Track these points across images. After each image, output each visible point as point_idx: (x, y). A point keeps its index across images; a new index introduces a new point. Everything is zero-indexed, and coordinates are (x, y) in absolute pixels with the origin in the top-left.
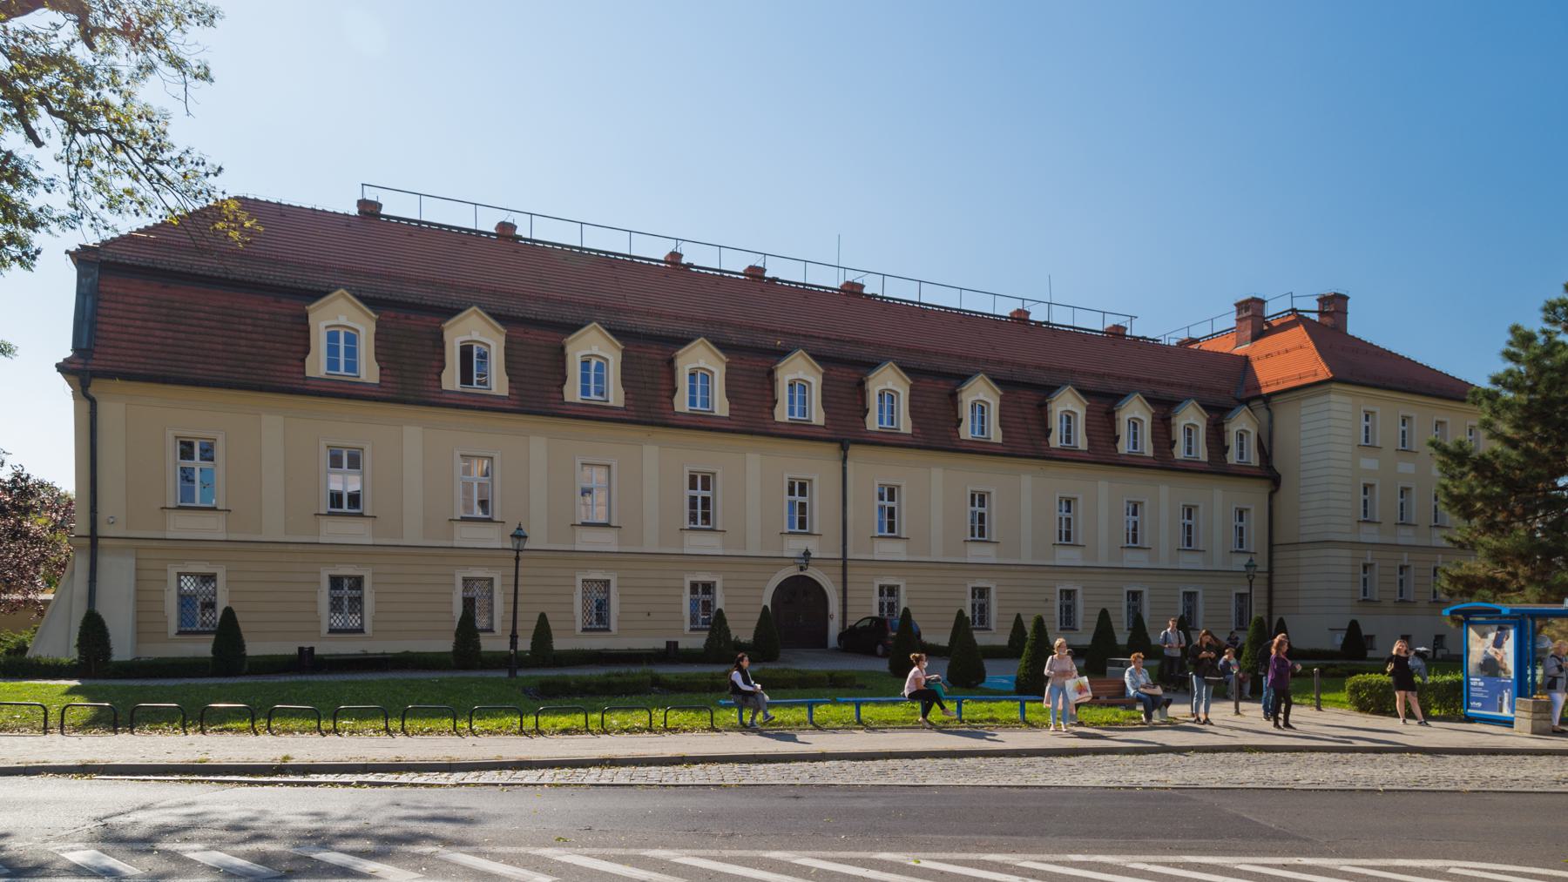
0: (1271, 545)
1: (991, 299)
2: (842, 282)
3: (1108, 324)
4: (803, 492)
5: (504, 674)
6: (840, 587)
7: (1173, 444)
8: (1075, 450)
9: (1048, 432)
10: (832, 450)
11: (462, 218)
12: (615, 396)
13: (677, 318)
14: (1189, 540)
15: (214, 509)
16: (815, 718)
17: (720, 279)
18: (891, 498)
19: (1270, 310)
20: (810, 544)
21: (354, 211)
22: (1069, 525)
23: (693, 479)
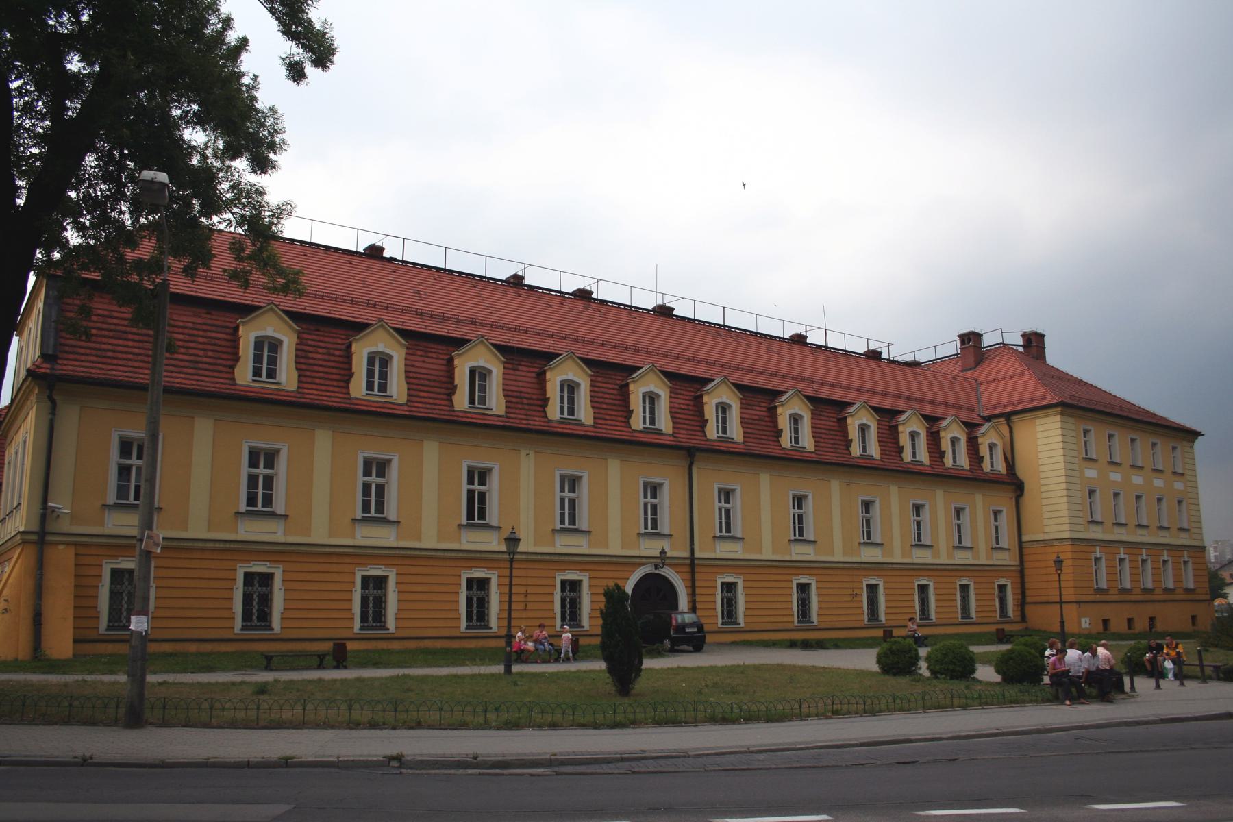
5: (499, 669)
9: (704, 422)
13: (832, 385)
19: (987, 341)
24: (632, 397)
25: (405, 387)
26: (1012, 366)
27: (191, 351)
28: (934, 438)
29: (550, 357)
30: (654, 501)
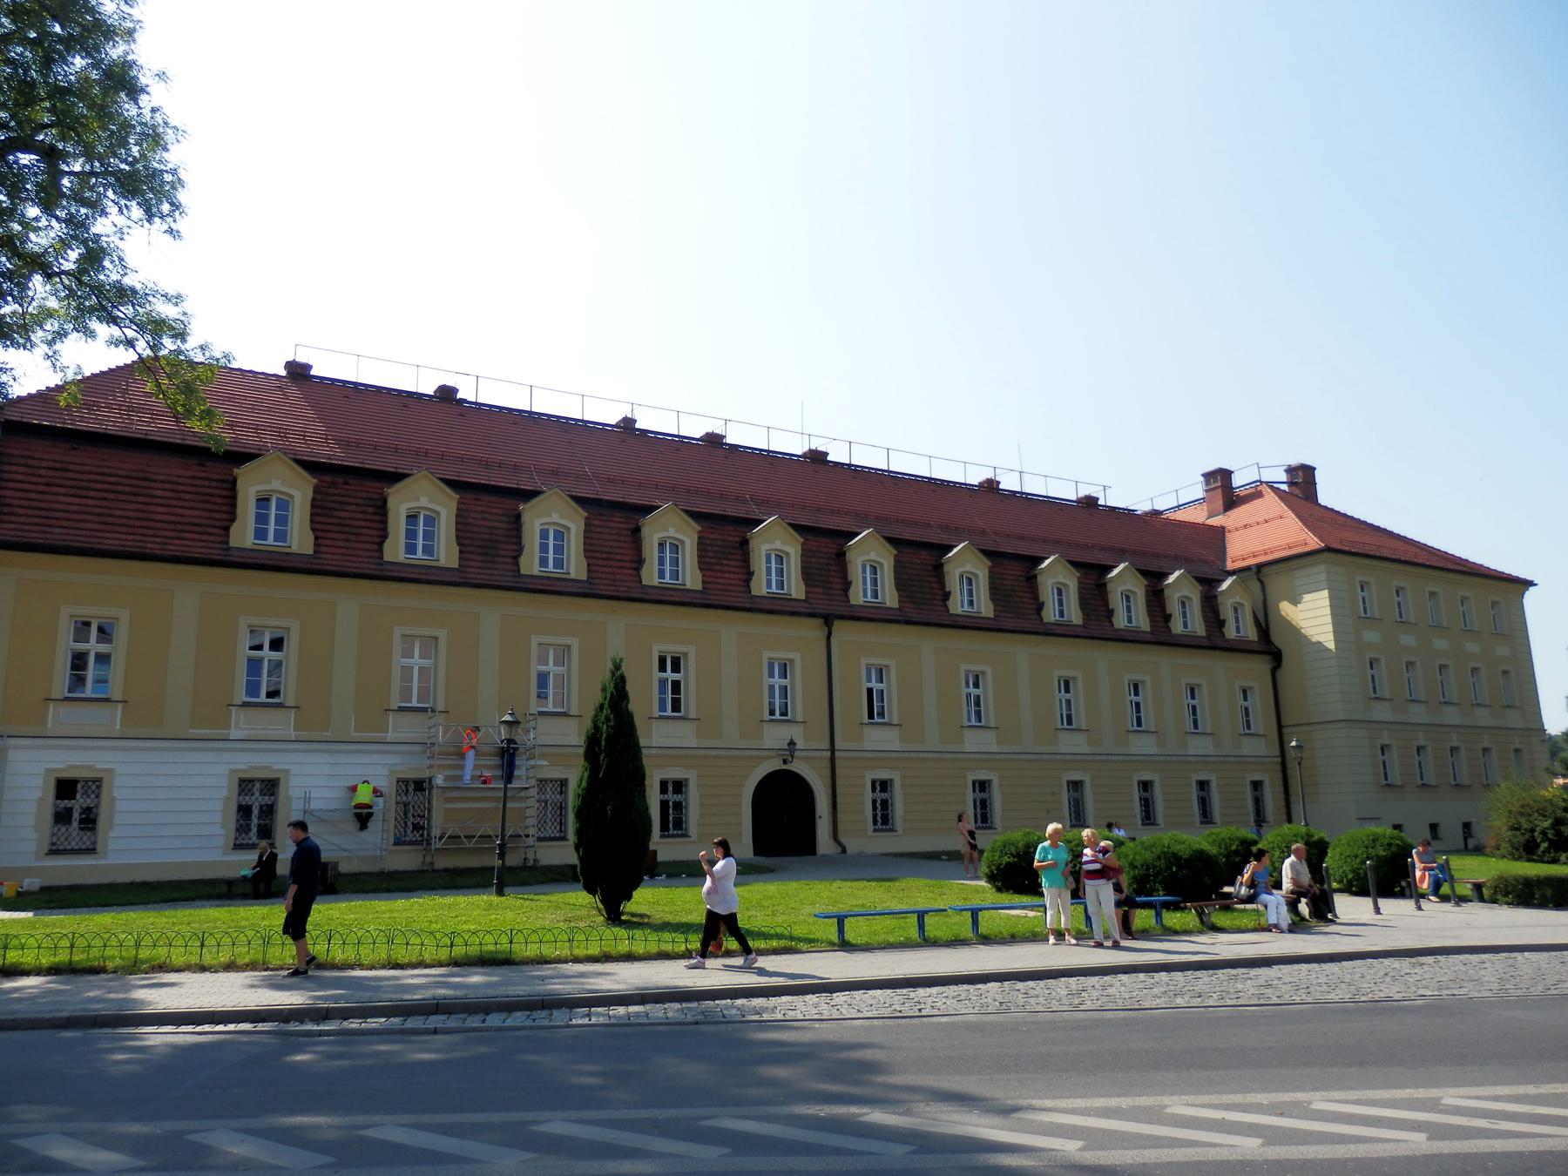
0: (1280, 727)
1: (961, 466)
2: (806, 449)
3: (1082, 494)
4: (676, 667)
6: (829, 781)
7: (1168, 618)
8: (1070, 625)
10: (811, 631)
11: (958, 477)
12: (576, 567)
13: (1021, 538)
14: (978, 713)
15: (107, 700)
16: (983, 930)
17: (679, 444)
18: (976, 685)
19: (1237, 480)
20: (796, 733)
21: (283, 373)
22: (1069, 708)
23: (662, 661)
24: (1110, 597)
25: (457, 548)
26: (1271, 505)
27: (172, 510)
28: (1156, 597)
29: (242, 457)
30: (676, 676)
